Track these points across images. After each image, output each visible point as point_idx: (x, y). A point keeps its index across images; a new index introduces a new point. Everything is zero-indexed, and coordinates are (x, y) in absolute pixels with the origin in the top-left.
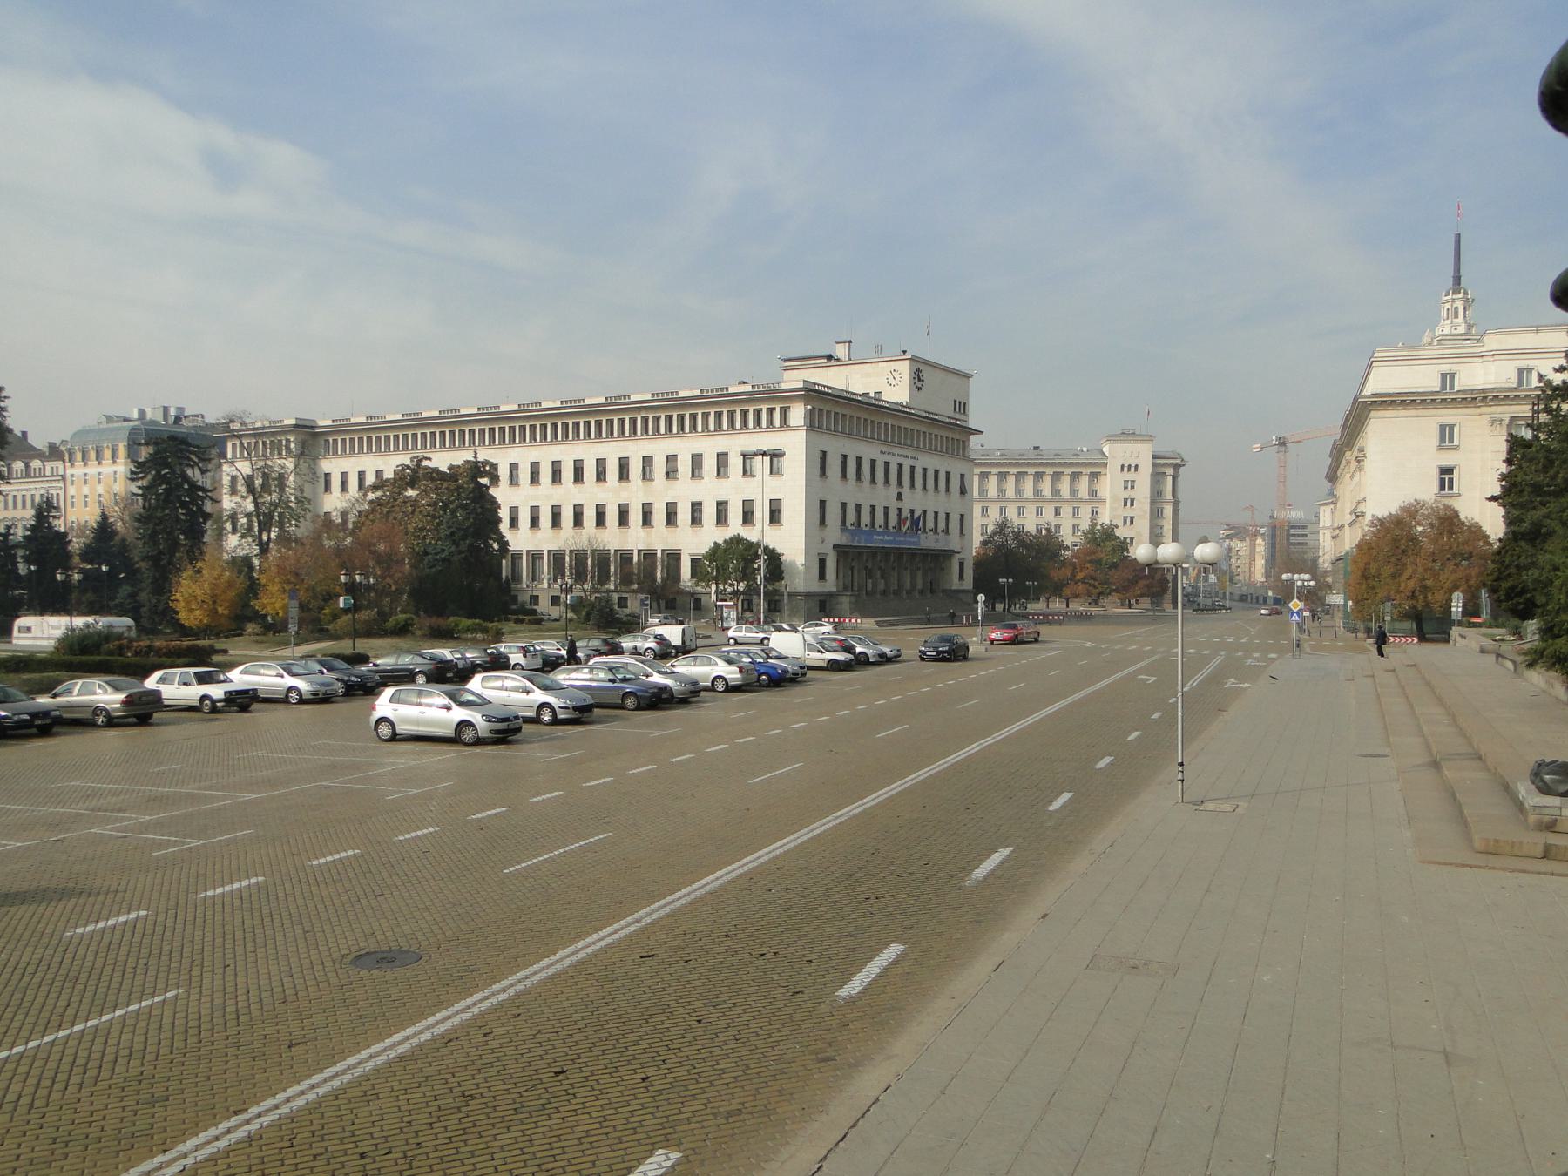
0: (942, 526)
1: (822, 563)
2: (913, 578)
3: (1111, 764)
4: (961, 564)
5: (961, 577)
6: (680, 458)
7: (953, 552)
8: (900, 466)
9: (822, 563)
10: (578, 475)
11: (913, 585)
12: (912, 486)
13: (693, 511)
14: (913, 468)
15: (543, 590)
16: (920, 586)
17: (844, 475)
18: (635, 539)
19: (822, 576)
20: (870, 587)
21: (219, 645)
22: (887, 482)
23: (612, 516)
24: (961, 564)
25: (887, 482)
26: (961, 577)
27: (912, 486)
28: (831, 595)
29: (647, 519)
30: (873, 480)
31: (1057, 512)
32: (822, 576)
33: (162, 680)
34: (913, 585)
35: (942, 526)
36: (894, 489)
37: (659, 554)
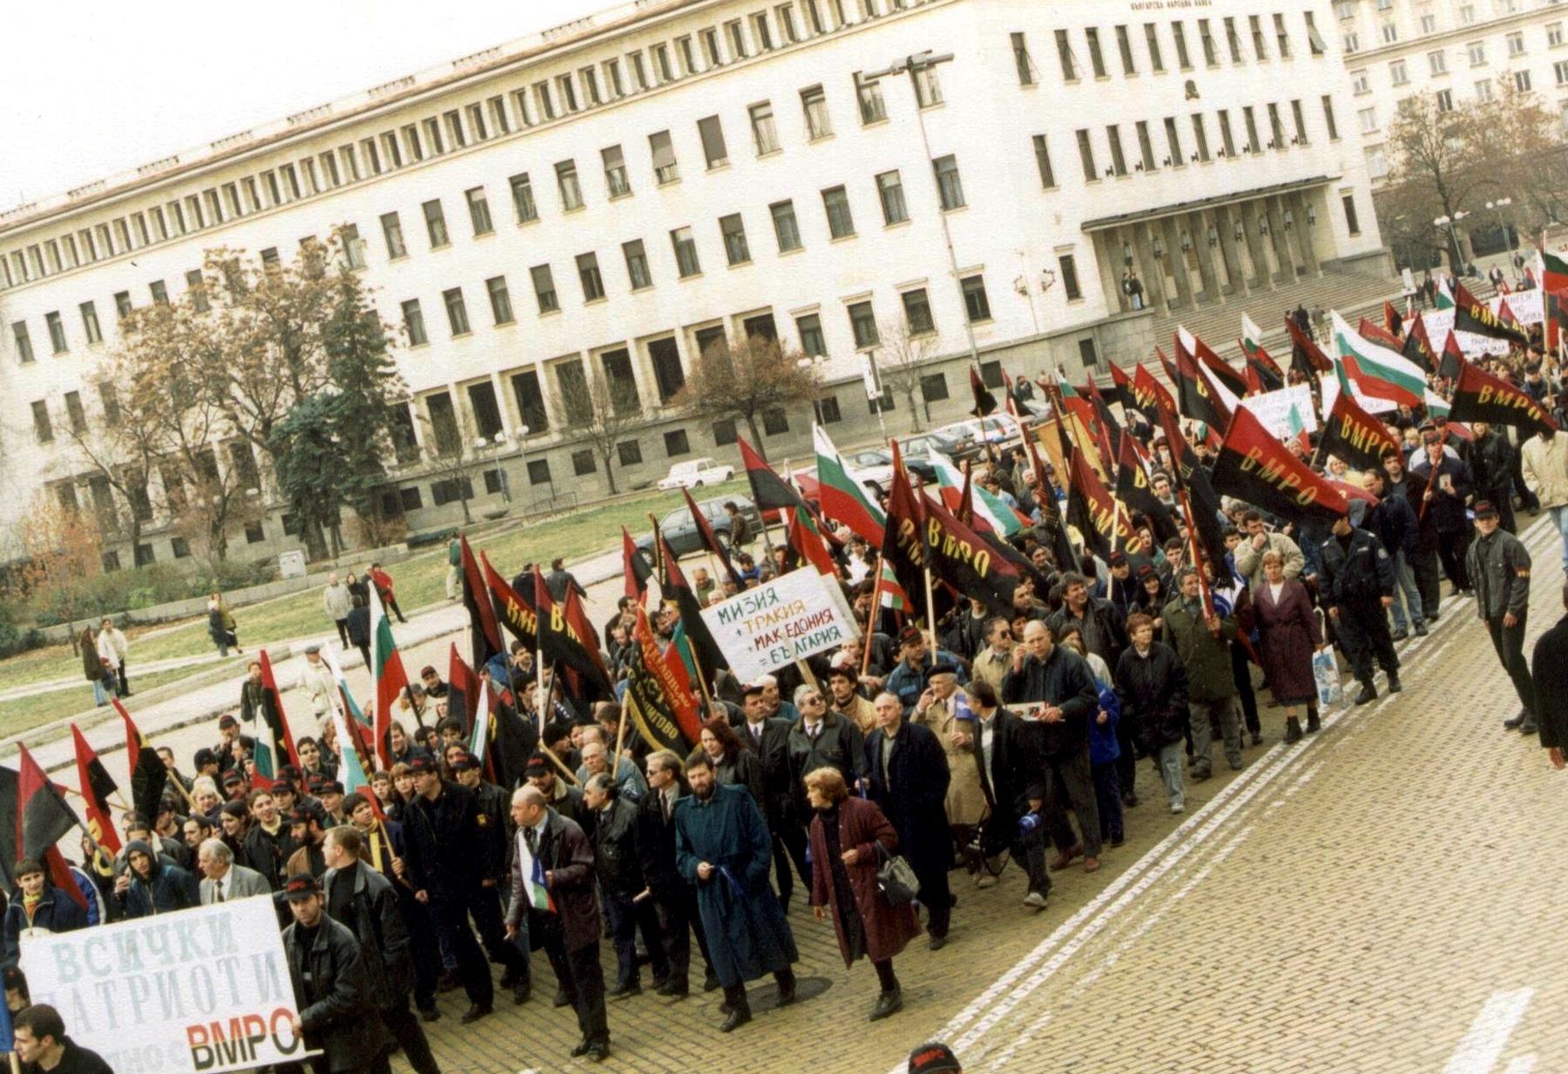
0: (1289, 130)
1: (1067, 264)
2: (1255, 251)
3: (1043, 726)
4: (1348, 203)
5: (1353, 227)
6: (675, 137)
7: (1324, 180)
8: (1177, 25)
9: (1067, 264)
10: (481, 218)
11: (1261, 269)
12: (1211, 59)
13: (778, 222)
14: (1204, 24)
15: (646, 428)
16: (1273, 266)
17: (1069, 73)
18: (674, 306)
19: (1073, 291)
20: (1172, 293)
21: (869, 494)
22: (1158, 65)
23: (613, 271)
24: (1348, 203)
25: (1158, 65)
26: (1353, 227)
27: (1211, 59)
28: (1100, 326)
29: (593, 285)
30: (1100, 70)
31: (1518, 46)
32: (1073, 291)
33: (1121, 515)
34: (1261, 269)
35: (1289, 130)
36: (1175, 77)
37: (216, 448)
